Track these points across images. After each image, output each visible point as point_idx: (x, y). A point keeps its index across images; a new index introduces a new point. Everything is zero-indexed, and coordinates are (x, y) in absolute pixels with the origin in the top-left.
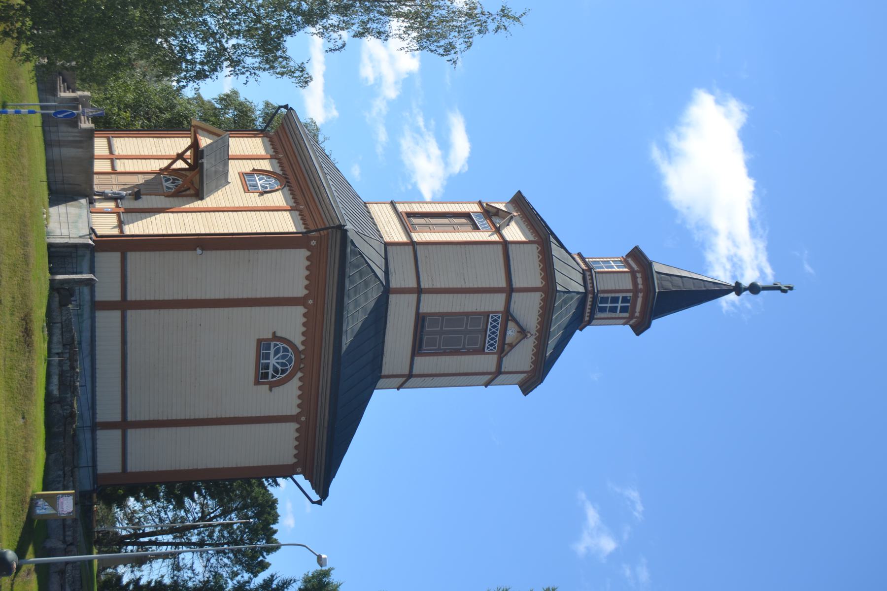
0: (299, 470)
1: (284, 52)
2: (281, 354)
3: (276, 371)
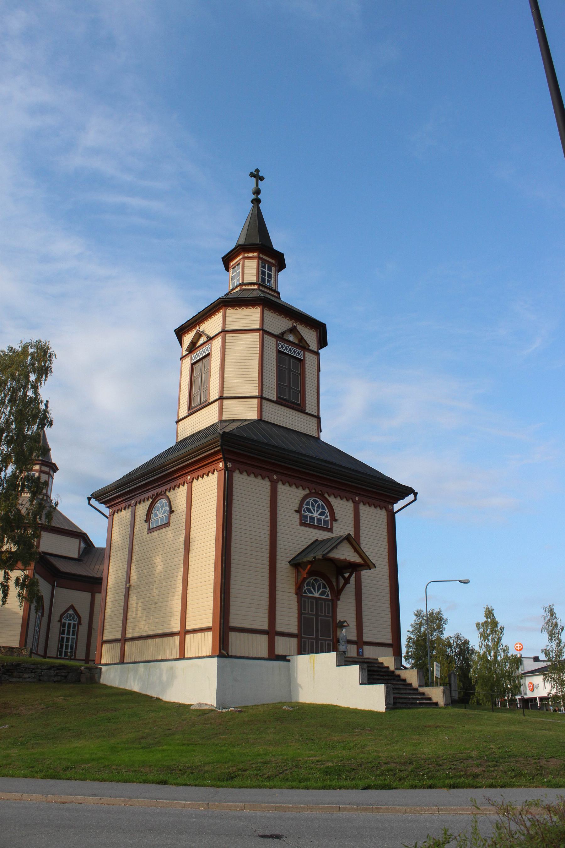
0: (390, 507)
1: (51, 363)
2: (311, 507)
3: (322, 514)
